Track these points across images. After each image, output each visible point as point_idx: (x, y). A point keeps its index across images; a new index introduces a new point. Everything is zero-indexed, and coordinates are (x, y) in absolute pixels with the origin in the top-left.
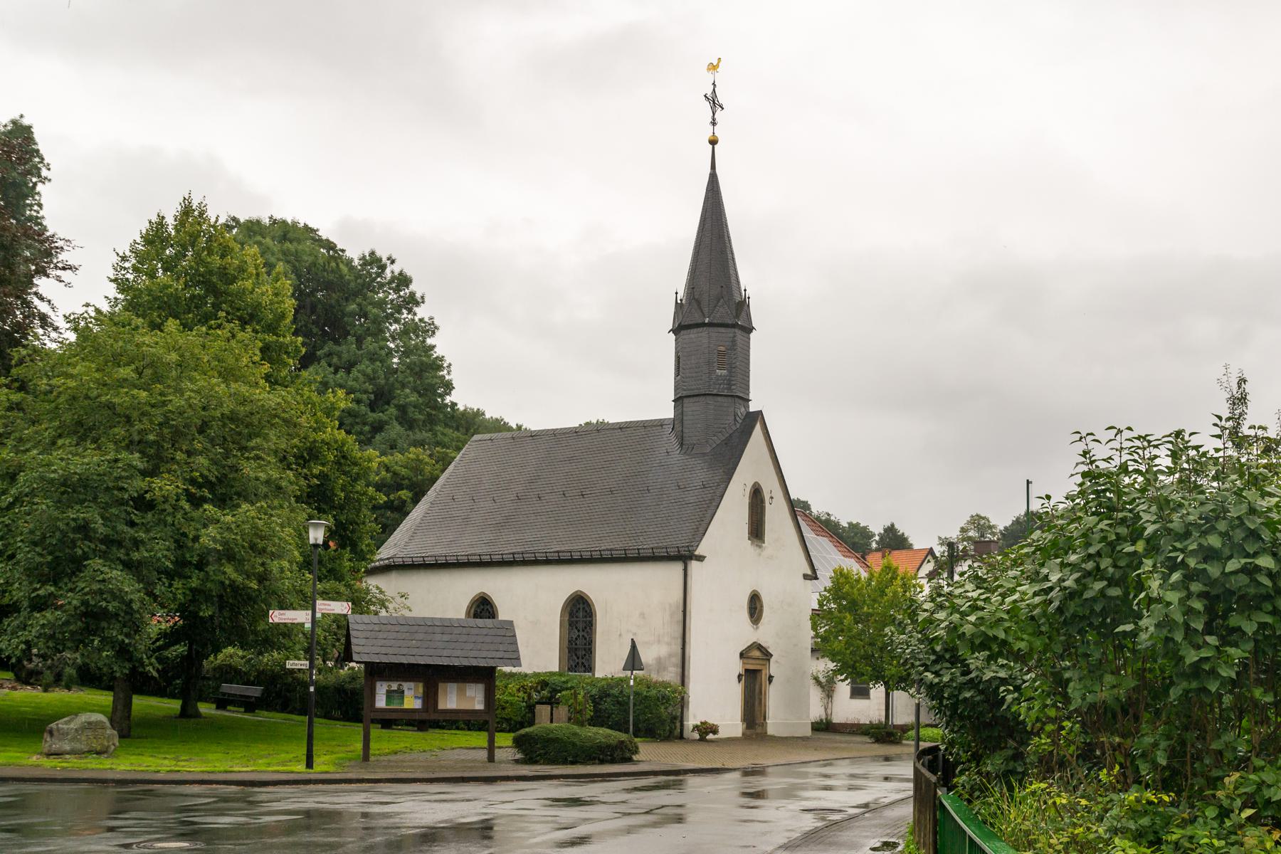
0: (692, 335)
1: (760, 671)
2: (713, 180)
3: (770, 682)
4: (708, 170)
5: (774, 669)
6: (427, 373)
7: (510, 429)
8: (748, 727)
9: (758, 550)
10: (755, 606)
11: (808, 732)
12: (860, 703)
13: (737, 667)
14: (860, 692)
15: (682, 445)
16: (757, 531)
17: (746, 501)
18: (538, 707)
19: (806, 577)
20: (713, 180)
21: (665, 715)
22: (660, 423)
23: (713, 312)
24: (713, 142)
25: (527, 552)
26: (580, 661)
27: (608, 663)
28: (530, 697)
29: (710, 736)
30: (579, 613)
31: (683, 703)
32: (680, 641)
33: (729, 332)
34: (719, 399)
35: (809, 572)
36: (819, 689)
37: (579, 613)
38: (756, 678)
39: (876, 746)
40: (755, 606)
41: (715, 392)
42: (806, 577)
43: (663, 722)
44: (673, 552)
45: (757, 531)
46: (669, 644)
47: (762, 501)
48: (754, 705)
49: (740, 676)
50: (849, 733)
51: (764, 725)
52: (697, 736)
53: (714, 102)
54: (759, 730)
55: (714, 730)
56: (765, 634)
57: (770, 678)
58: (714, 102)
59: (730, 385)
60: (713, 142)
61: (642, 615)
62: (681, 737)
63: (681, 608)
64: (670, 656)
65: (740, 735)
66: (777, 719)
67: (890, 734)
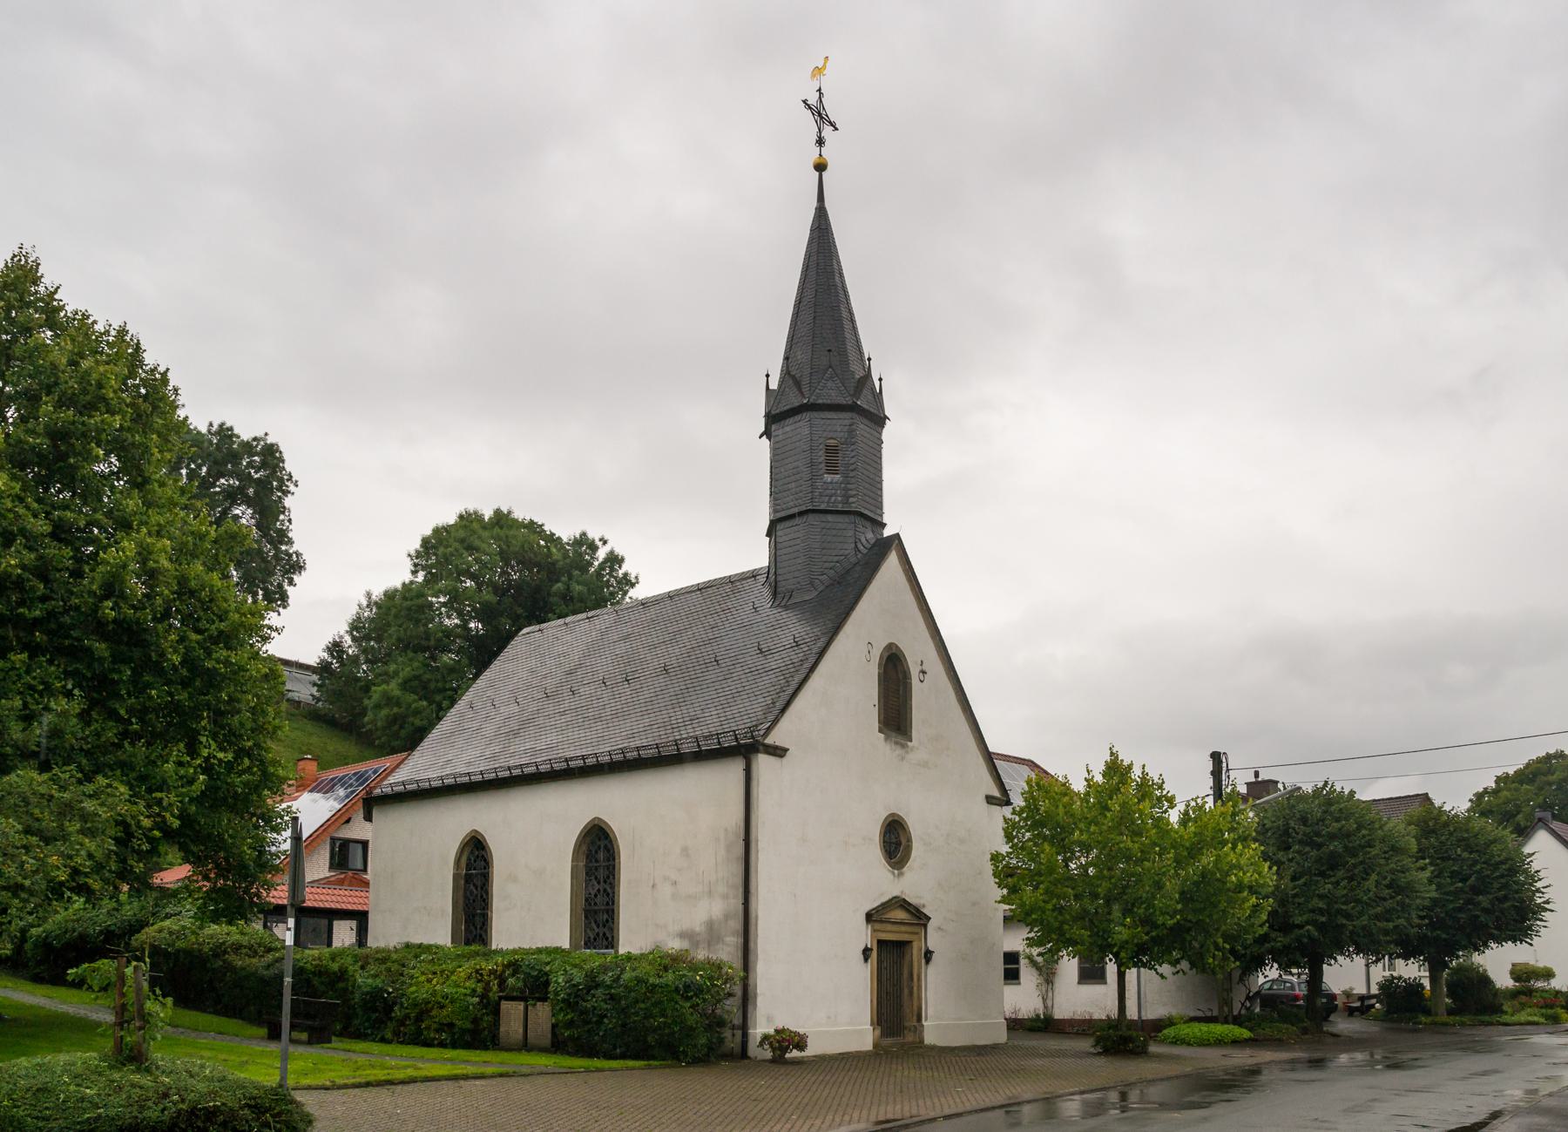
0: (786, 429)
1: (910, 942)
2: (821, 216)
3: (928, 961)
4: (815, 204)
5: (934, 940)
8: (884, 1034)
9: (899, 751)
10: (895, 840)
11: (1002, 1036)
12: (1092, 991)
13: (863, 936)
14: (1091, 974)
15: (775, 594)
17: (874, 670)
18: (505, 1005)
19: (990, 800)
20: (821, 216)
21: (692, 1019)
22: (753, 575)
23: (825, 404)
24: (820, 167)
26: (601, 930)
27: (637, 933)
28: (487, 988)
29: (795, 1053)
30: (597, 851)
31: (747, 999)
33: (839, 422)
34: (830, 518)
35: (996, 793)
36: (1034, 972)
37: (597, 851)
38: (902, 956)
39: (1102, 1061)
40: (895, 840)
41: (823, 507)
42: (990, 800)
43: (690, 1032)
44: (728, 742)
46: (725, 897)
47: (906, 675)
48: (900, 997)
49: (866, 953)
50: (1077, 1034)
51: (918, 1029)
52: (769, 1054)
53: (820, 114)
54: (910, 1038)
55: (800, 1043)
56: (915, 883)
57: (928, 955)
58: (820, 114)
59: (847, 497)
60: (820, 167)
61: (685, 851)
62: (744, 1054)
64: (727, 917)
65: (867, 1045)
66: (944, 1014)
67: (1126, 1040)
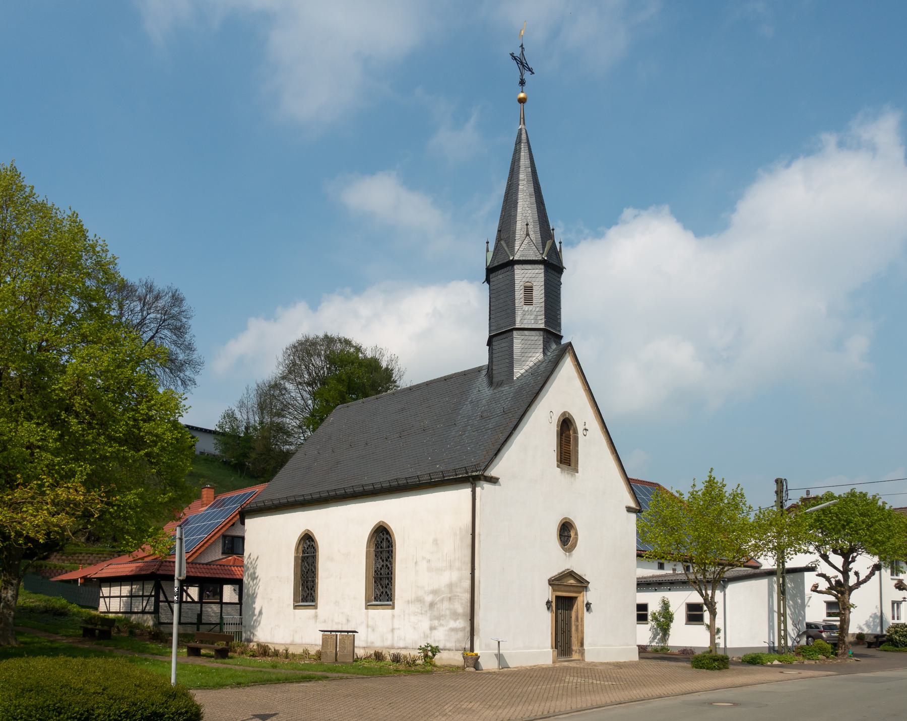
6: (105, 270)
7: (835, 498)
10: (566, 532)
11: (635, 657)
13: (548, 594)
16: (567, 455)
25: (307, 495)
32: (469, 565)
40: (566, 532)
45: (567, 455)
46: (459, 569)
49: (549, 603)
56: (579, 561)
61: (436, 542)
63: (470, 532)
